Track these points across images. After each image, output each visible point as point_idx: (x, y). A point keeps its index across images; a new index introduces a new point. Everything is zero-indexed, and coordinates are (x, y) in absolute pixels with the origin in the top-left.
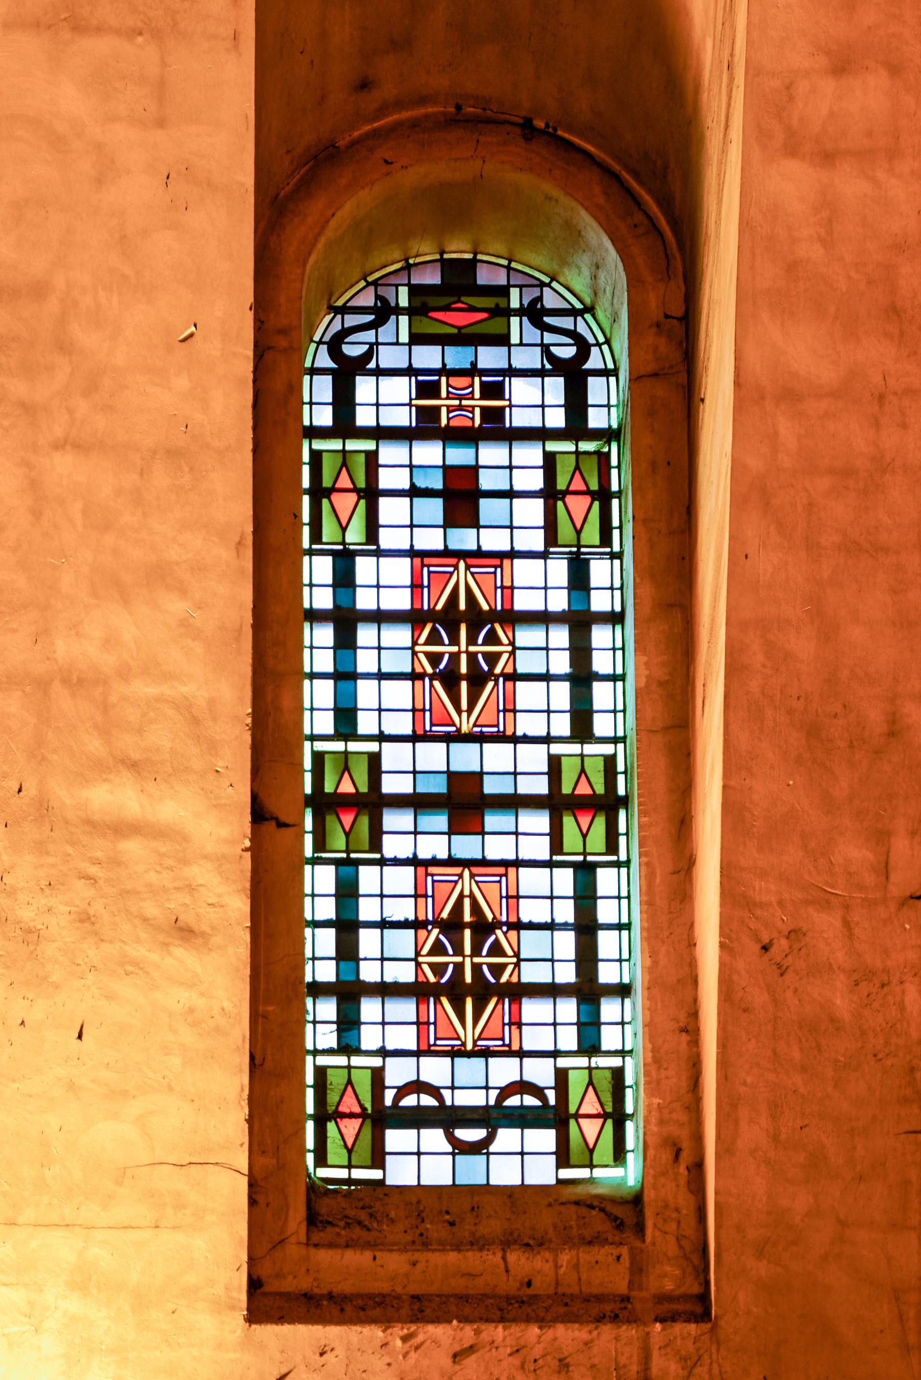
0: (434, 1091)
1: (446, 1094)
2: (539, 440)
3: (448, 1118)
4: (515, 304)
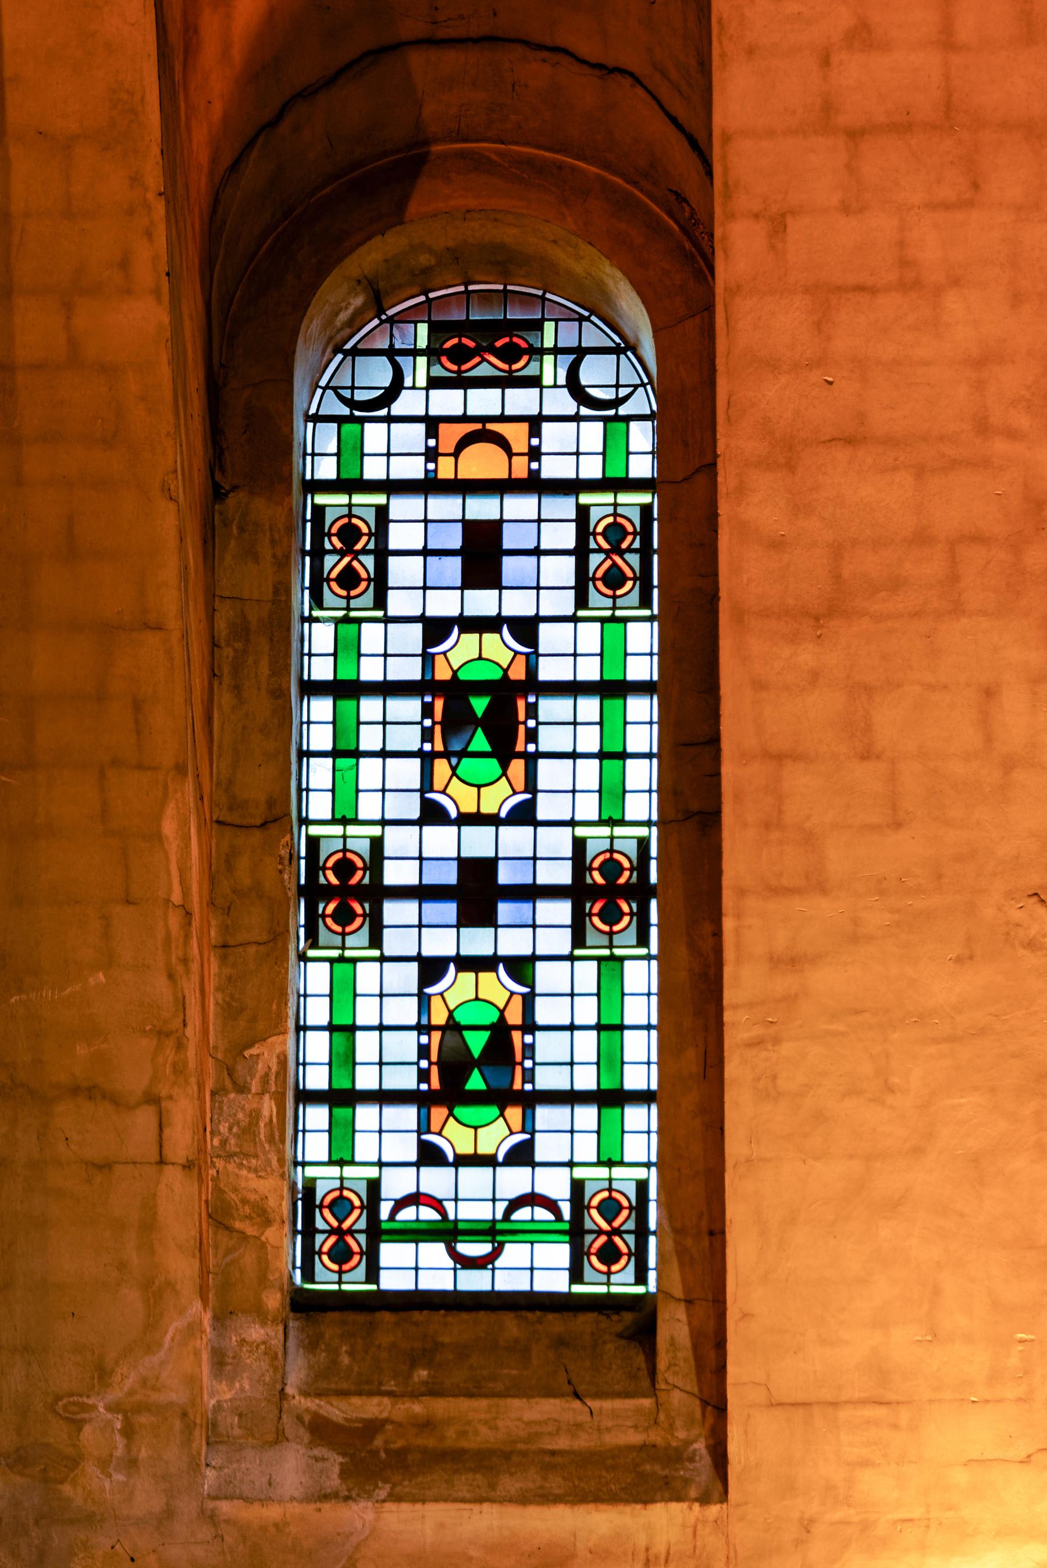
0: (436, 1204)
1: (449, 1206)
2: (570, 696)
3: (448, 1233)
4: (549, 343)
